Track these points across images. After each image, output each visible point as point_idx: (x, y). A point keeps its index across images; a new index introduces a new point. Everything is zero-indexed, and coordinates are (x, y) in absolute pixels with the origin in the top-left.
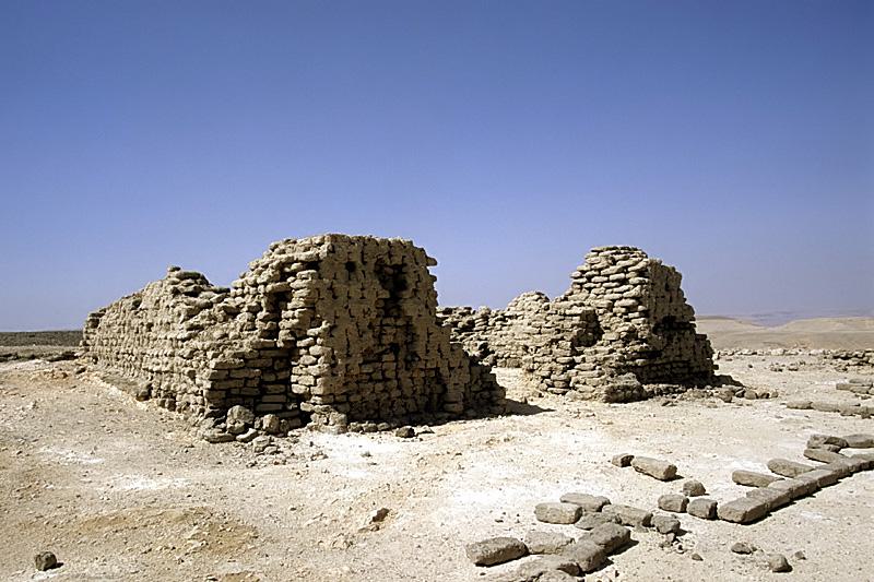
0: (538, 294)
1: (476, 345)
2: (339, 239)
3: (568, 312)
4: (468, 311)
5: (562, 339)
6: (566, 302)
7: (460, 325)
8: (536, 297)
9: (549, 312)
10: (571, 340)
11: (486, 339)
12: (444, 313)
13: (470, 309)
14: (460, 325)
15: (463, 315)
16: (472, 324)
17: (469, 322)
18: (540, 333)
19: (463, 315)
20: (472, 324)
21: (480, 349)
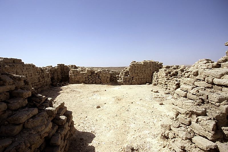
0: (207, 60)
1: (175, 83)
2: (15, 62)
3: (216, 81)
4: (178, 67)
5: (204, 114)
6: (217, 70)
7: (171, 73)
8: (205, 61)
9: (198, 77)
10: (217, 119)
11: (180, 81)
12: (166, 68)
13: (178, 66)
14: (171, 73)
15: (175, 69)
16: (177, 73)
17: (175, 72)
18: (186, 97)
19: (175, 69)
20: (177, 73)
21: (176, 85)
